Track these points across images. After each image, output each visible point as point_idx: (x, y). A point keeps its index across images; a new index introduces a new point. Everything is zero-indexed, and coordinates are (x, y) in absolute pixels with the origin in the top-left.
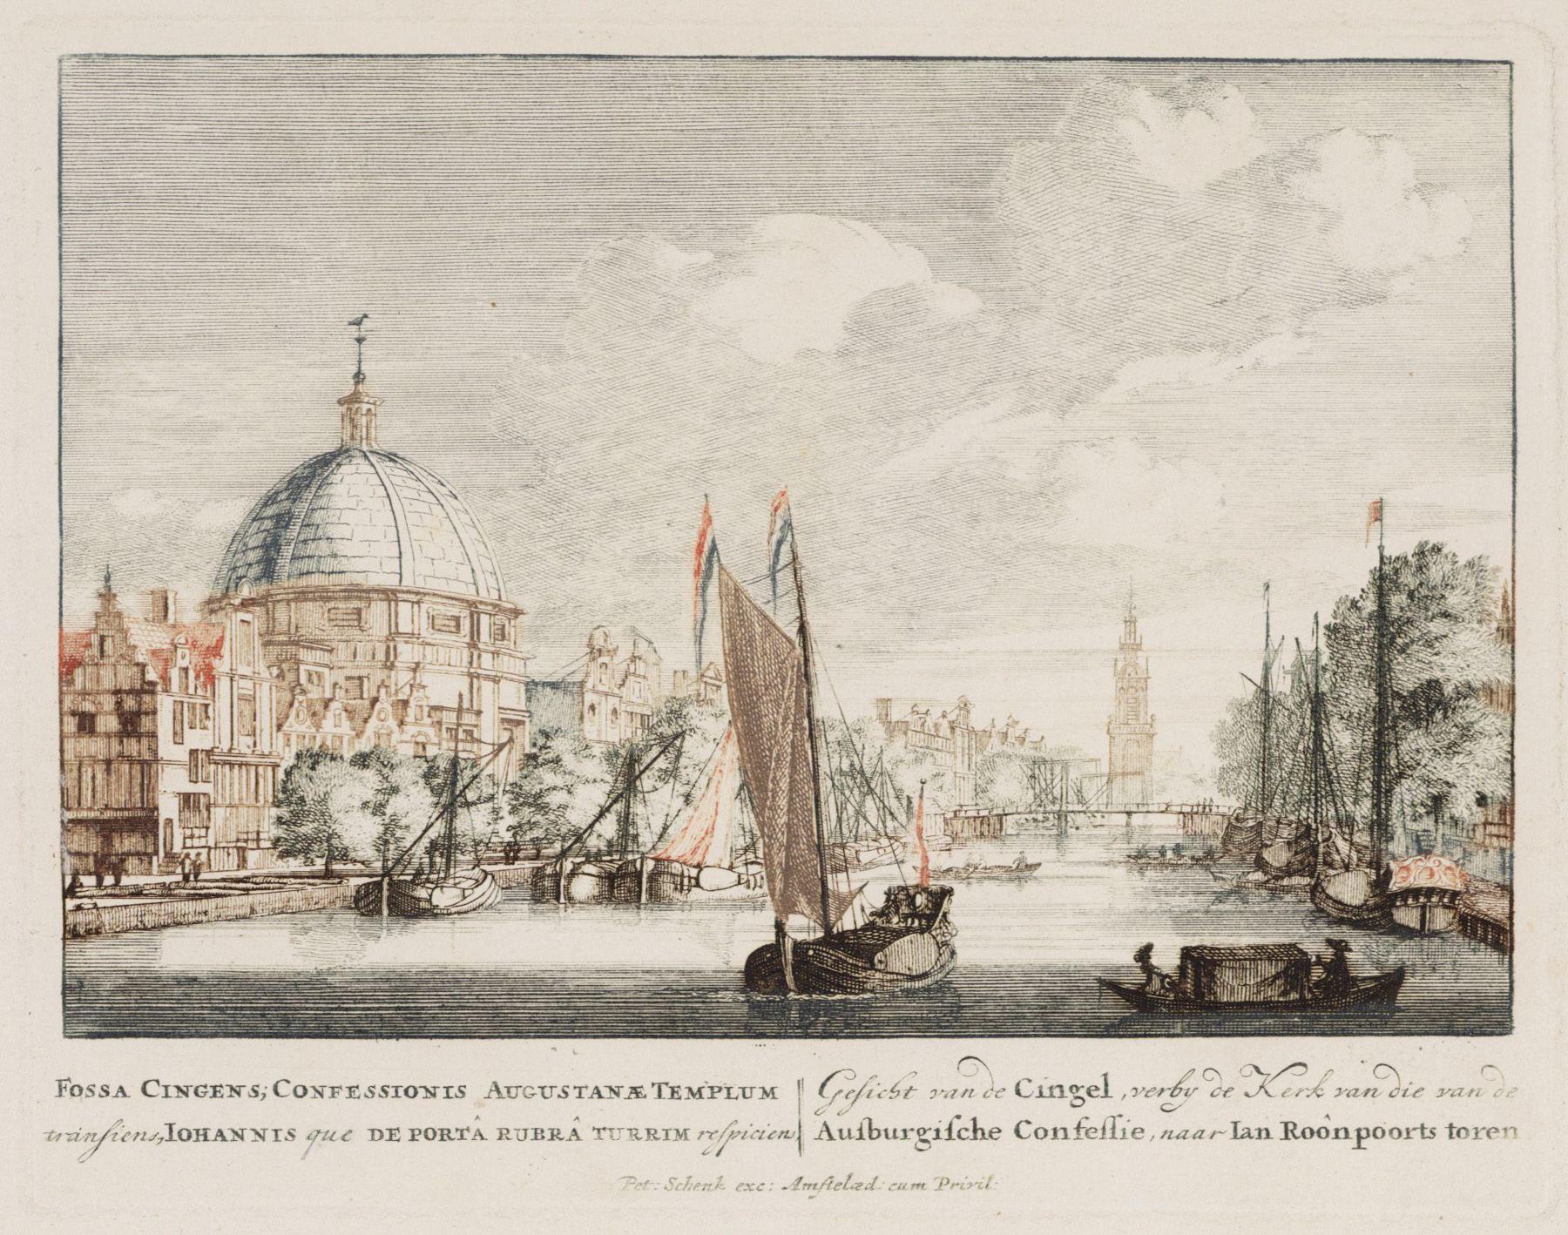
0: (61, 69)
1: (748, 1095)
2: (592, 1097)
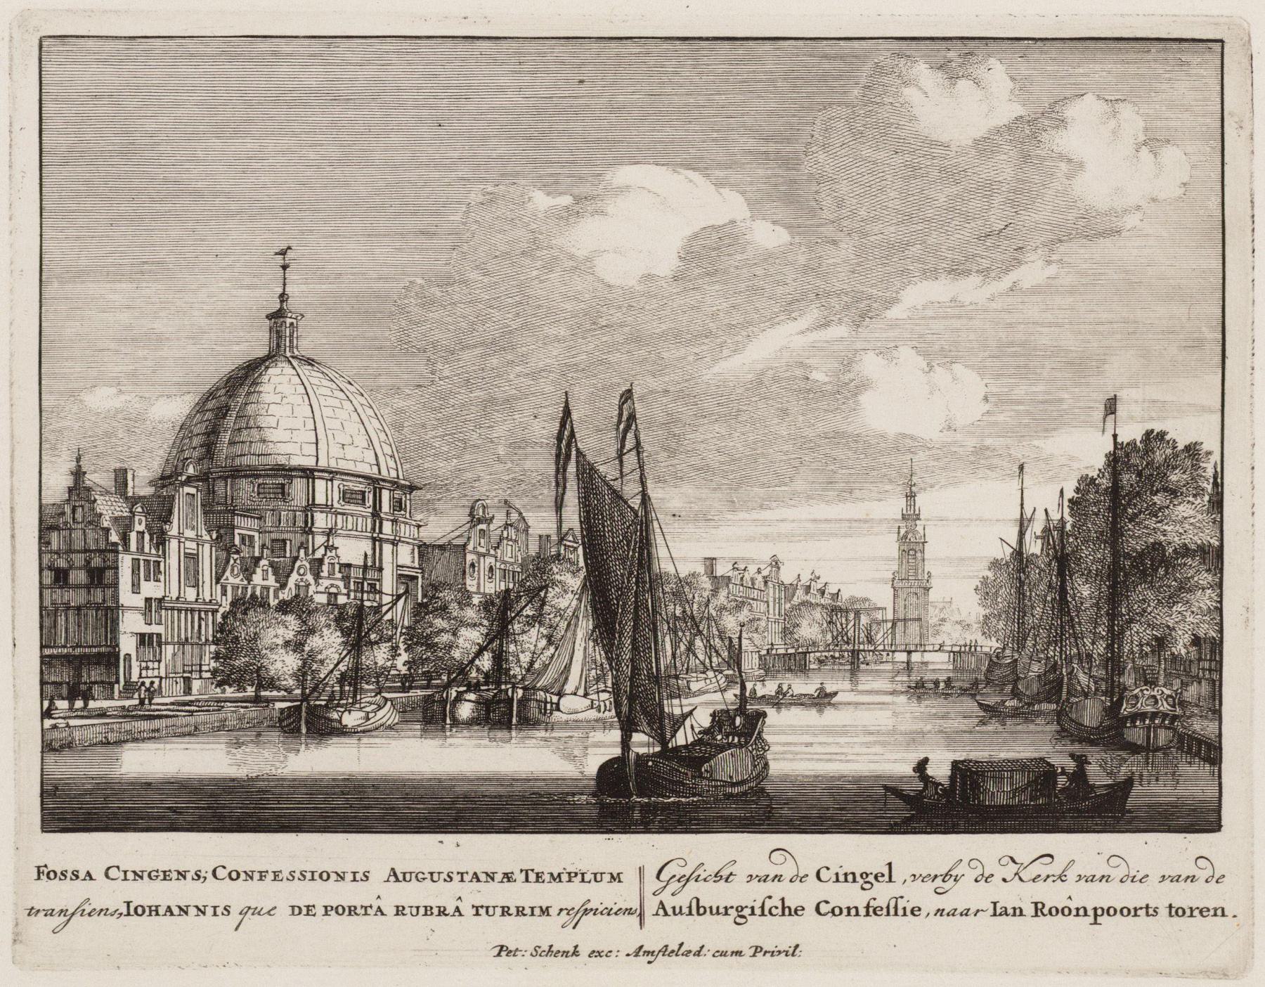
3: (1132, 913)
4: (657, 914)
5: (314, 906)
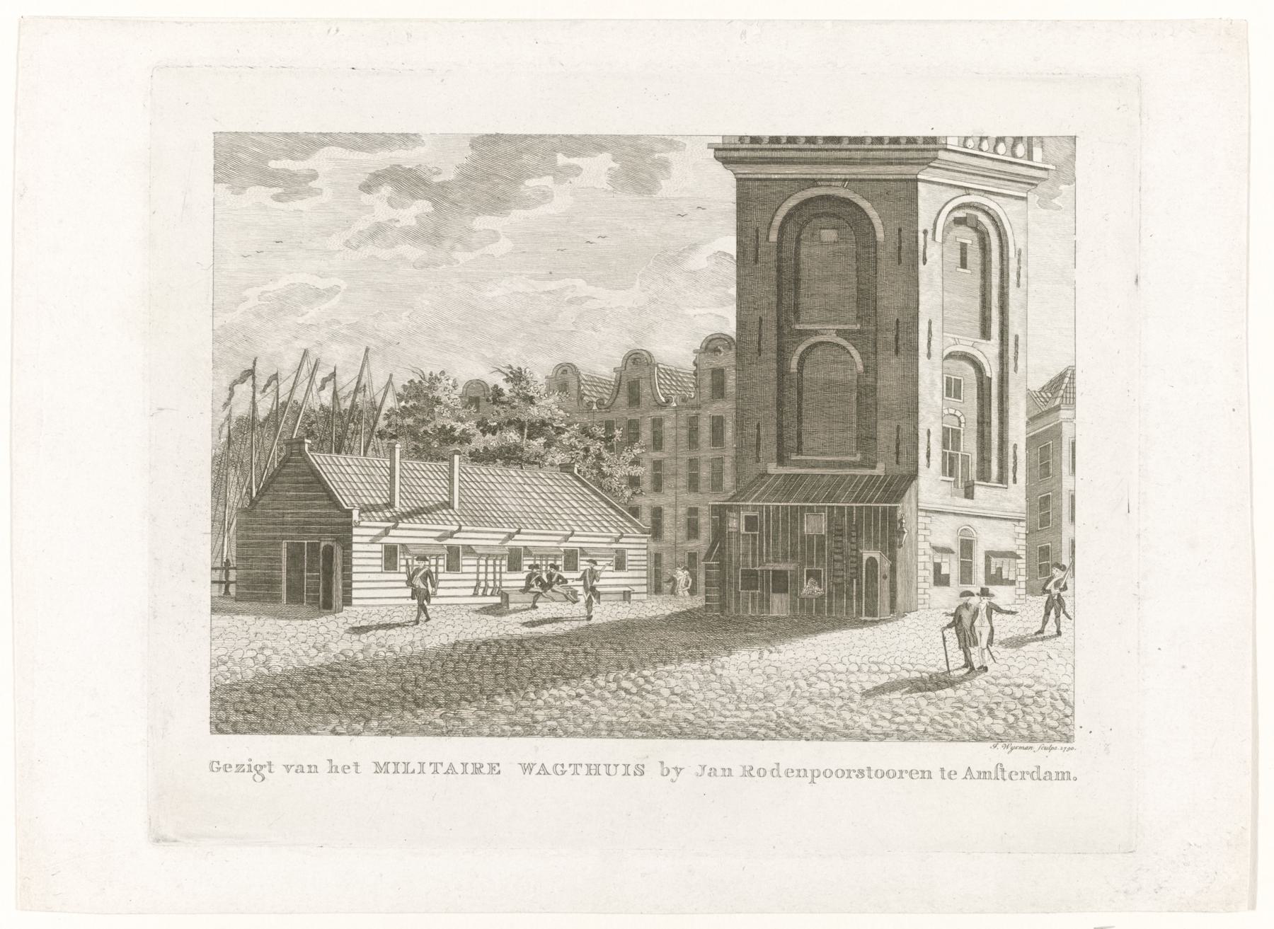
0: (72, 19)
1: (612, 772)
2: (965, 778)
3: (846, 775)
4: (965, 778)
5: (498, 764)
